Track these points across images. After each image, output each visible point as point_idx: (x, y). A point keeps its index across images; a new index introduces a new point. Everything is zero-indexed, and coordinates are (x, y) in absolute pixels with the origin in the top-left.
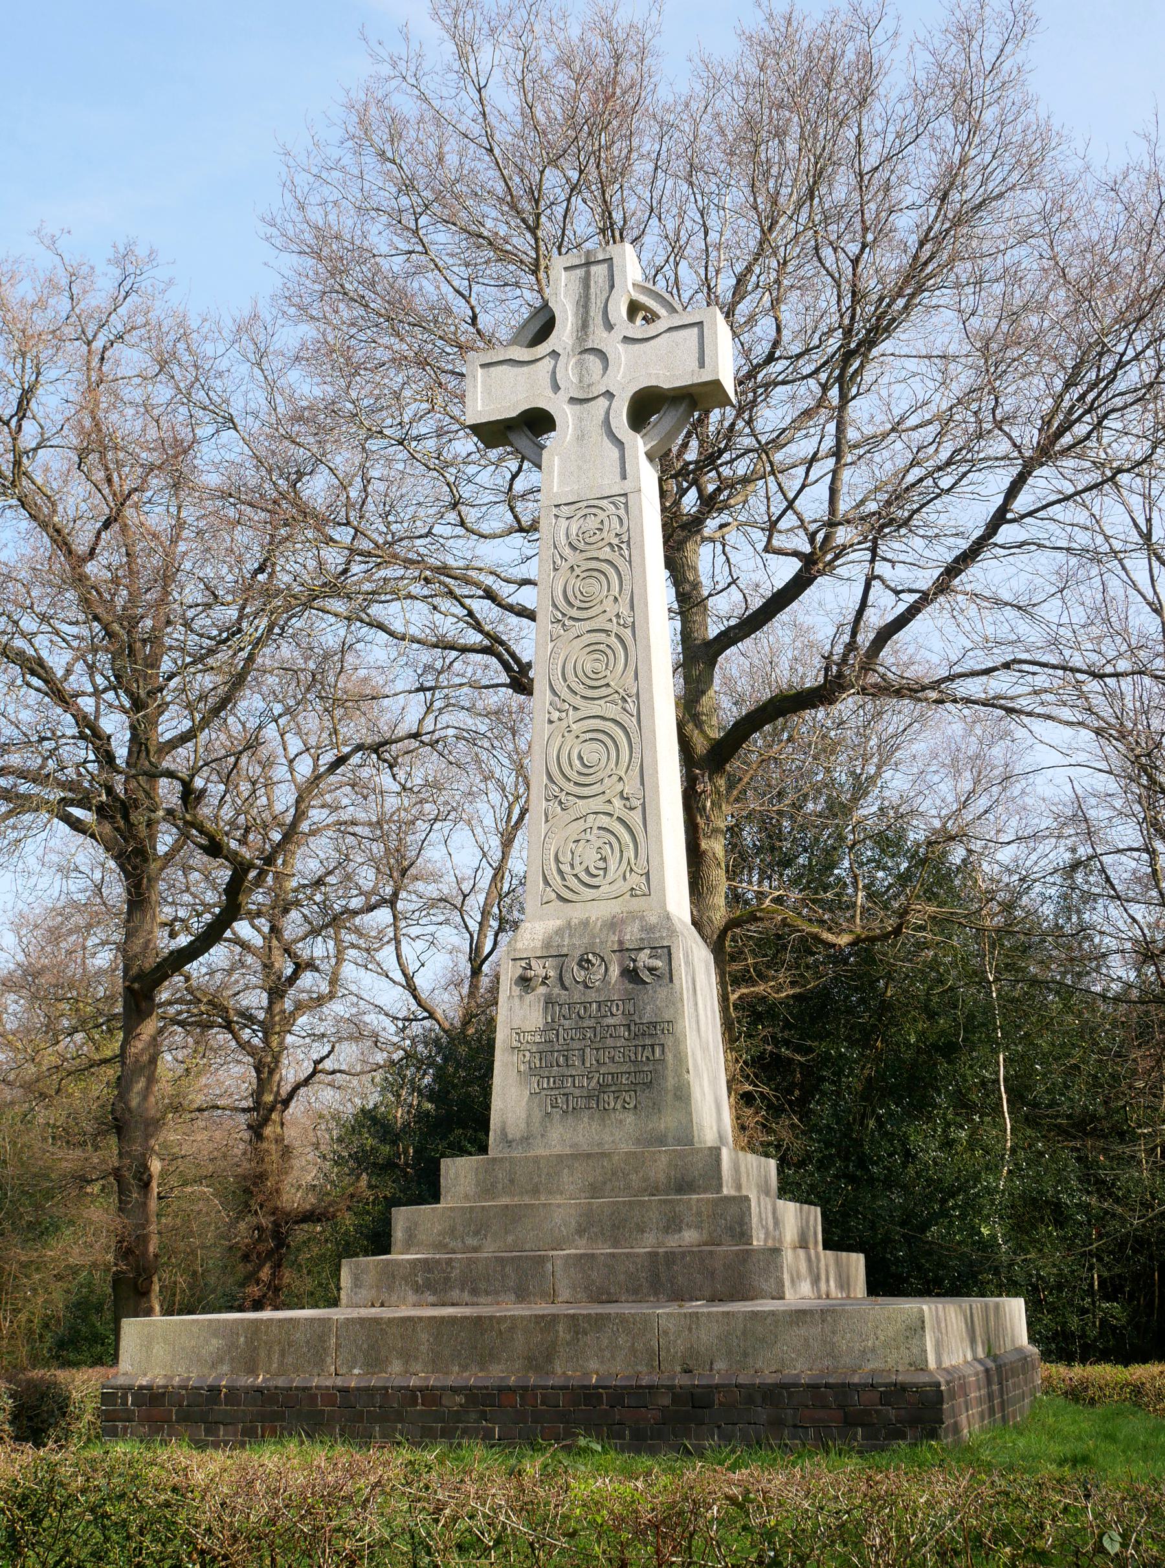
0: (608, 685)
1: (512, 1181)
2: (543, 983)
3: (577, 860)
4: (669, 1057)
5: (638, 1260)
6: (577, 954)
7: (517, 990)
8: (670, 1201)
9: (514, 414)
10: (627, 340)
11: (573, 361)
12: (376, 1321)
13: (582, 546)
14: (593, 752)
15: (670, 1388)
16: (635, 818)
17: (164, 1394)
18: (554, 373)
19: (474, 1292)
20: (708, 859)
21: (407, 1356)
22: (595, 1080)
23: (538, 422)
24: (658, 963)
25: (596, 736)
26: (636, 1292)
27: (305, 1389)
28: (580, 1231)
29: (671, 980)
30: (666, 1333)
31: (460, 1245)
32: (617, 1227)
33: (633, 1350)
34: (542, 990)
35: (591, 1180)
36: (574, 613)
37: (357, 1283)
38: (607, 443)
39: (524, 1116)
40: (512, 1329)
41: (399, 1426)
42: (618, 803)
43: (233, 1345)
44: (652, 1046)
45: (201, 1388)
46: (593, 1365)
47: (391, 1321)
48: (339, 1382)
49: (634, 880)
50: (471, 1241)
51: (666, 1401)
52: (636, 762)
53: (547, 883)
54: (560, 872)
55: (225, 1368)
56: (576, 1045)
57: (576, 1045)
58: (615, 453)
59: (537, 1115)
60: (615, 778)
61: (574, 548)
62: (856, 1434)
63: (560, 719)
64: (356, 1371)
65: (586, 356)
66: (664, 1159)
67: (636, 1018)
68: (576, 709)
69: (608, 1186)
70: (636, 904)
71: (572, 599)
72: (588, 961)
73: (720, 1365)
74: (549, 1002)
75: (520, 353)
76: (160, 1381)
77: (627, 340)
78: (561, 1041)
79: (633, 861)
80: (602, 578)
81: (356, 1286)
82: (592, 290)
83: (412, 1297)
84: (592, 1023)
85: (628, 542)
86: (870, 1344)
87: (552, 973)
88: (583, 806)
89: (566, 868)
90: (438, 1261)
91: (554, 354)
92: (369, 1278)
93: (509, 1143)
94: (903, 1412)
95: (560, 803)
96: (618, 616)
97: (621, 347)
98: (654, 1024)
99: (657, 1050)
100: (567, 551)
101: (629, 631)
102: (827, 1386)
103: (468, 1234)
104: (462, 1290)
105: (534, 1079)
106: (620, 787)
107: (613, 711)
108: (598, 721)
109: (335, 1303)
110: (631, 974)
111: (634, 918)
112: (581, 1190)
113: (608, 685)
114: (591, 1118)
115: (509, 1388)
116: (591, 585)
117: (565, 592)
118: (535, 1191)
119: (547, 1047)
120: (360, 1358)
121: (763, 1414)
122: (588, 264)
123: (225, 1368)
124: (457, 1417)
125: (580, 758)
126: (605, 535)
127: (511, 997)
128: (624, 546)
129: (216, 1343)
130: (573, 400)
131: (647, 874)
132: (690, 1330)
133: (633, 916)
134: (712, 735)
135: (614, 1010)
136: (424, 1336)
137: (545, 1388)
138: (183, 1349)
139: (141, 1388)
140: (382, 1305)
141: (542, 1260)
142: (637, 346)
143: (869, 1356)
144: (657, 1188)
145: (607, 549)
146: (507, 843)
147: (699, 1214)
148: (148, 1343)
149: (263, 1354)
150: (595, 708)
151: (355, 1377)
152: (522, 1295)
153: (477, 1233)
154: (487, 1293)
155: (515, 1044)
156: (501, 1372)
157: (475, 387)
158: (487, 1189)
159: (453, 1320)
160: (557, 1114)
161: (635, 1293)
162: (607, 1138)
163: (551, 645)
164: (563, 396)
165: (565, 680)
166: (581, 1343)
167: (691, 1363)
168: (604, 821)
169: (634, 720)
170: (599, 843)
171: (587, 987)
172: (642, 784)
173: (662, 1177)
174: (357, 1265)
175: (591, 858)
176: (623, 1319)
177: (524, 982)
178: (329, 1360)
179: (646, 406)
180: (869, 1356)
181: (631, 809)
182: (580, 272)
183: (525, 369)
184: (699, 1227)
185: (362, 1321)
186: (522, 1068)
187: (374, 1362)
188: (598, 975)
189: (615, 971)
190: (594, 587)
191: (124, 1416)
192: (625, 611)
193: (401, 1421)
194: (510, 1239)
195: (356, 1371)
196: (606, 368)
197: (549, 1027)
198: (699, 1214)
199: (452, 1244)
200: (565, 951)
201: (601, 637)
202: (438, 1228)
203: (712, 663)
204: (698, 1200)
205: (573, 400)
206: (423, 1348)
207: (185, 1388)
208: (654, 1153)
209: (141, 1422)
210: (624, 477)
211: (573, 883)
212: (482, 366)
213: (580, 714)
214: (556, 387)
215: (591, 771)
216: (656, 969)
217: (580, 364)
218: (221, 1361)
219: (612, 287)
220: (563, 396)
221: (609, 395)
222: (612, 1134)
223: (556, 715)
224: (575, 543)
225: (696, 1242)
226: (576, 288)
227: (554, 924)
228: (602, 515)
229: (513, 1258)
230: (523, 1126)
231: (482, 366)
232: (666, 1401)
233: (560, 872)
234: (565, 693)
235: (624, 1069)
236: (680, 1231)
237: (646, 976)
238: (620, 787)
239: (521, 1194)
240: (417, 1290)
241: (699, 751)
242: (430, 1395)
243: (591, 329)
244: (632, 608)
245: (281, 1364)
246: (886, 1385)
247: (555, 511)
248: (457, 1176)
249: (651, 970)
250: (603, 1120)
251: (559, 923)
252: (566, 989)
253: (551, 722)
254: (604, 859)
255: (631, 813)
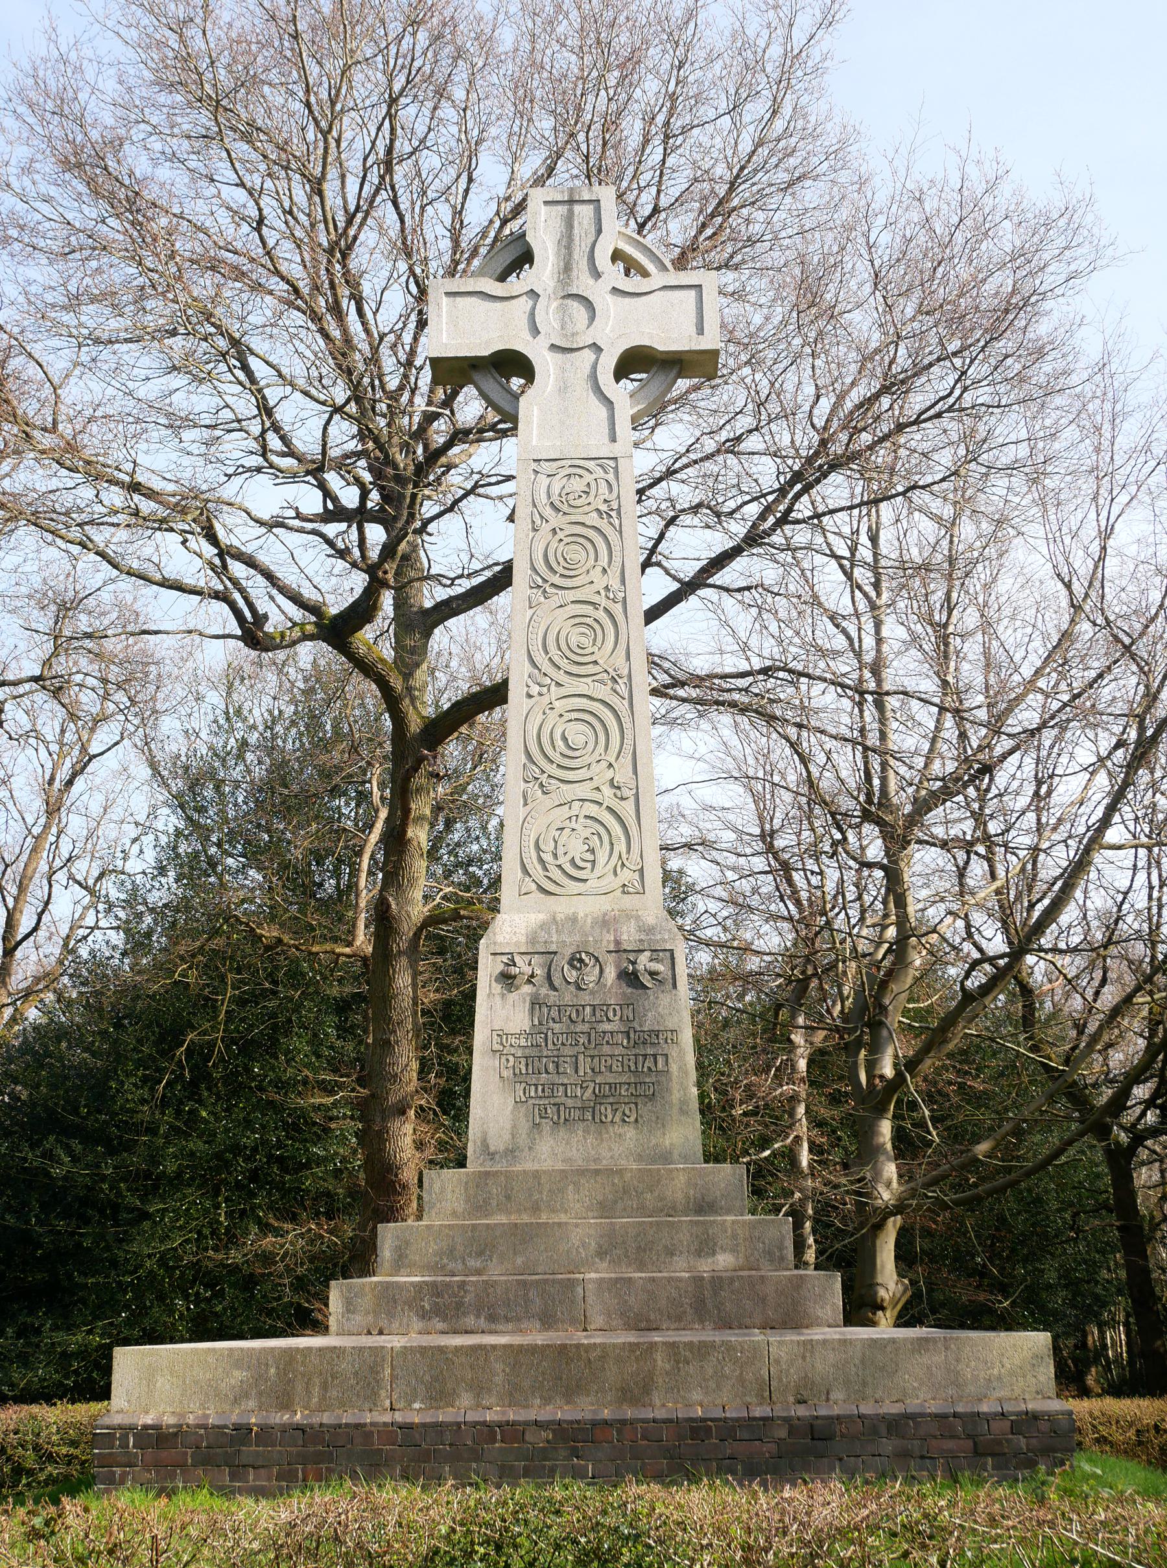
0: (595, 662)
1: (508, 1198)
2: (529, 982)
3: (560, 851)
4: (674, 1068)
5: (681, 1285)
6: (568, 952)
7: (497, 988)
8: (703, 1223)
9: (486, 353)
10: (615, 291)
11: (555, 304)
12: (441, 1349)
13: (565, 508)
14: (578, 734)
15: (787, 1420)
16: (627, 809)
17: (176, 1434)
18: (532, 314)
19: (492, 1318)
20: (412, 848)
21: (479, 1389)
22: (590, 1090)
23: (511, 364)
24: (660, 967)
25: (583, 716)
26: (679, 1319)
27: (358, 1426)
28: (601, 1253)
29: (675, 986)
30: (777, 1362)
31: (460, 1267)
32: (642, 1251)
33: (741, 1380)
34: (527, 989)
35: (600, 1198)
36: (557, 580)
37: (350, 1307)
38: (593, 400)
39: (508, 1126)
40: (603, 1357)
41: (474, 1465)
42: (607, 791)
43: (259, 1378)
44: (655, 1056)
45: (225, 1427)
46: (696, 1396)
47: (458, 1349)
48: (399, 1417)
49: (626, 876)
50: (473, 1263)
51: (783, 1433)
52: (628, 748)
53: (526, 871)
54: (541, 861)
55: (252, 1404)
56: (567, 1051)
57: (567, 1051)
58: (603, 412)
59: (524, 1126)
60: (604, 764)
61: (558, 510)
62: (986, 1464)
63: (540, 694)
64: (417, 1406)
65: (569, 302)
66: (682, 1178)
67: (636, 1025)
68: (558, 684)
69: (620, 1205)
70: (628, 902)
71: (554, 565)
72: (581, 961)
73: (838, 1395)
74: (536, 1003)
76: (172, 1420)
77: (615, 291)
78: (550, 1046)
79: (624, 856)
80: (589, 546)
81: (348, 1311)
82: (576, 231)
83: (417, 1324)
84: (585, 1028)
85: (619, 513)
86: (996, 1372)
87: (538, 972)
88: (568, 791)
89: (548, 858)
90: (448, 1285)
91: (533, 294)
92: (366, 1302)
93: (492, 1156)
94: (1034, 1441)
95: (541, 785)
96: (607, 588)
97: (610, 299)
98: (657, 1033)
99: (660, 1060)
100: (548, 512)
101: (619, 606)
102: (955, 1415)
103: (470, 1255)
104: (478, 1317)
105: (520, 1088)
106: (610, 774)
107: (603, 692)
108: (584, 700)
109: (320, 1327)
110: (630, 978)
111: (629, 917)
112: (589, 1209)
113: (595, 662)
114: (586, 1131)
115: (606, 1422)
116: (576, 552)
117: (546, 556)
118: (536, 1209)
119: (534, 1052)
120: (421, 1389)
121: (888, 1446)
122: (571, 202)
123: (252, 1404)
124: (544, 1454)
125: (564, 739)
126: (591, 499)
127: (490, 995)
128: (613, 514)
129: (239, 1375)
130: (553, 347)
131: (641, 870)
132: (804, 1358)
133: (628, 915)
134: (425, 714)
135: (611, 1014)
136: (499, 1367)
137: (644, 1421)
138: (196, 1382)
139: (146, 1427)
140: (381, 1333)
141: (571, 1284)
142: (627, 300)
143: (995, 1384)
144: (674, 1208)
145: (595, 514)
146: (53, 809)
147: (734, 1236)
148: (149, 1375)
149: (299, 1387)
150: (582, 687)
151: (416, 1413)
152: (548, 1321)
153: (480, 1254)
154: (507, 1320)
155: (497, 1047)
157: (439, 316)
158: (479, 1207)
160: (547, 1125)
161: (678, 1320)
162: (605, 1153)
163: (530, 612)
164: (543, 342)
165: (547, 653)
166: (682, 1373)
167: (806, 1394)
168: (593, 810)
169: (626, 702)
170: (587, 833)
171: (579, 988)
172: (635, 772)
173: (679, 1195)
174: (350, 1288)
175: (577, 849)
176: (729, 1347)
177: (507, 979)
178: (383, 1393)
180: (995, 1384)
181: (622, 799)
182: (562, 209)
183: (498, 305)
184: (734, 1250)
185: (423, 1350)
186: (505, 1074)
187: (439, 1395)
188: (591, 975)
189: (611, 974)
190: (576, 554)
191: (124, 1460)
192: (615, 584)
193: (477, 1459)
194: (519, 1261)
195: (417, 1406)
196: (592, 318)
198: (734, 1236)
199: (451, 1266)
200: (553, 948)
201: (588, 610)
202: (433, 1247)
203: (428, 634)
204: (733, 1222)
205: (553, 347)
206: (498, 1379)
207: (205, 1427)
208: (671, 1171)
209: (146, 1467)
210: (613, 440)
211: (556, 874)
212: (448, 294)
213: (563, 691)
214: (535, 331)
215: (577, 754)
216: (657, 973)
217: (562, 309)
218: (247, 1396)
219: (599, 231)
220: (543, 342)
221: (596, 348)
222: (610, 1149)
223: (535, 689)
224: (557, 503)
225: (731, 1267)
227: (536, 918)
228: (588, 478)
229: (537, 1281)
230: (507, 1136)
231: (448, 294)
232: (783, 1433)
233: (541, 861)
234: (546, 667)
235: (624, 1079)
236: (714, 1254)
237: (646, 980)
238: (610, 774)
239: (519, 1211)
240: (424, 1315)
241: (412, 729)
242: (512, 1431)
243: (574, 273)
244: (623, 582)
245: (323, 1398)
246: (1018, 1414)
247: (534, 465)
248: (443, 1190)
249: (653, 974)
250: (600, 1133)
251: (542, 917)
252: (556, 990)
253: (530, 696)
254: (592, 851)
255: (623, 803)
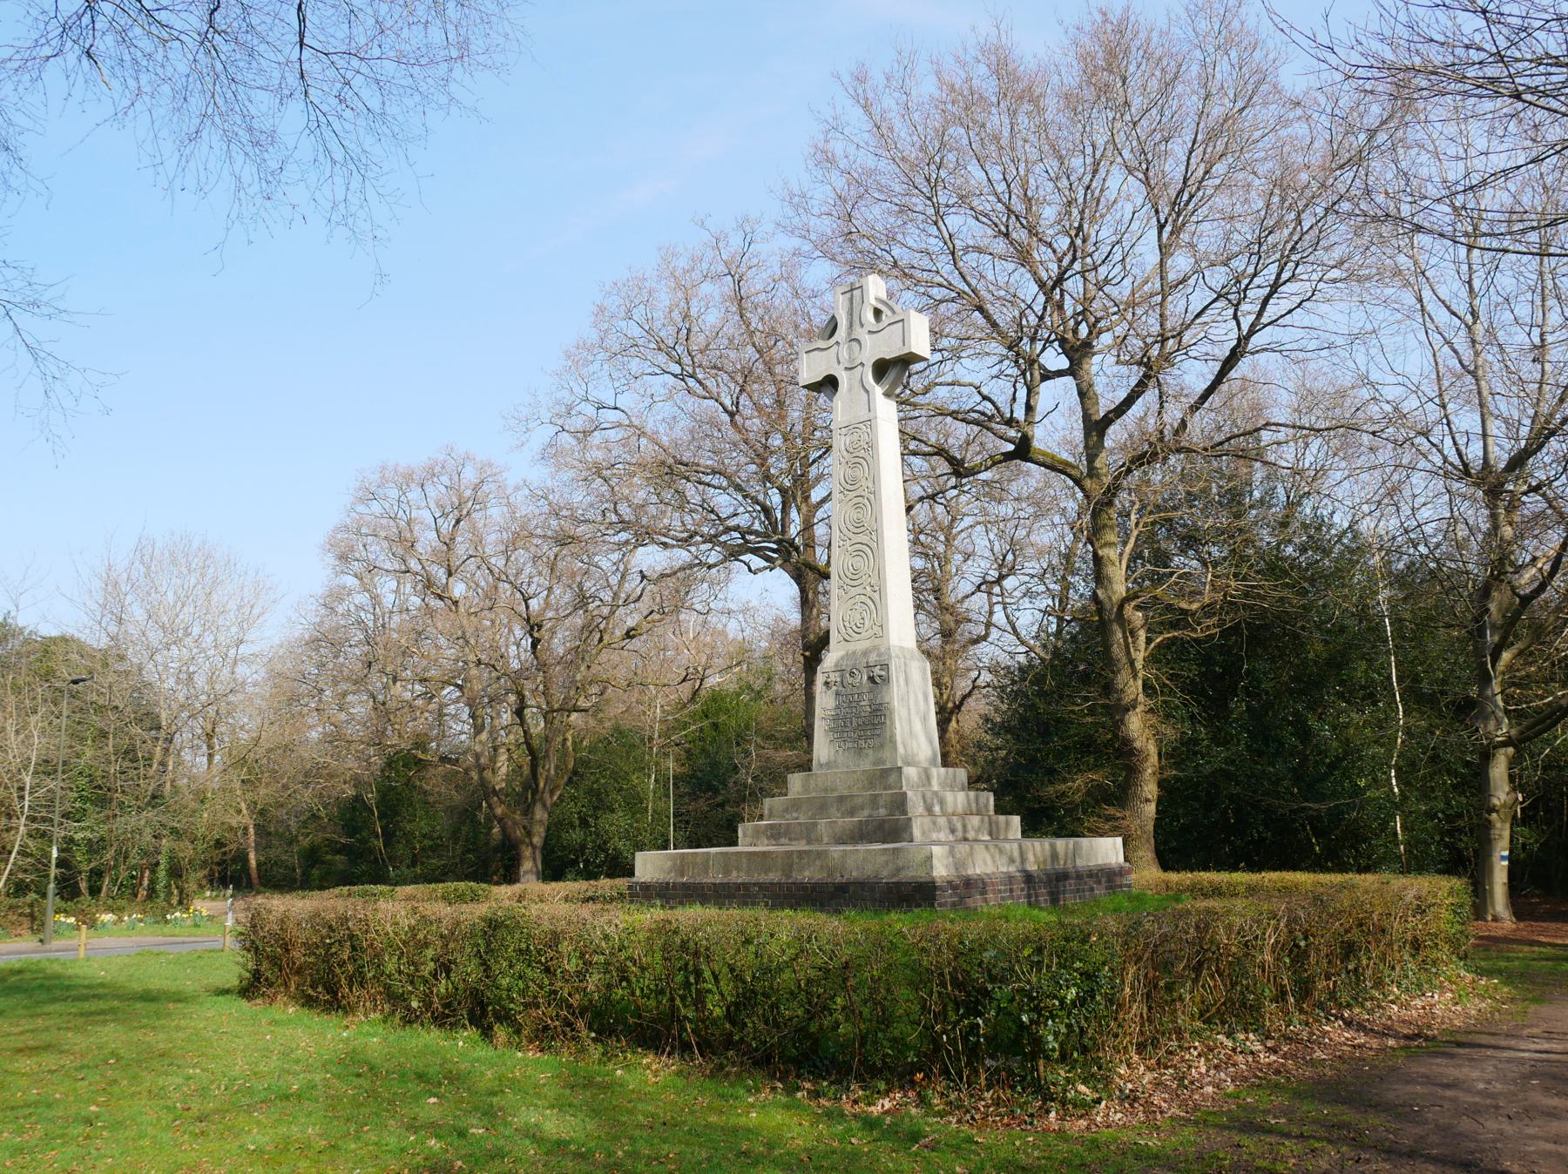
14: (858, 562)
16: (876, 596)
21: (738, 870)
37: (745, 835)
74: (837, 694)
75: (821, 344)
109: (735, 843)
151: (720, 878)
156: (774, 877)
159: (755, 853)
164: (842, 367)
179: (882, 369)
187: (727, 872)
197: (837, 707)
217: (850, 348)
226: (847, 303)
237: (878, 680)
242: (745, 886)
